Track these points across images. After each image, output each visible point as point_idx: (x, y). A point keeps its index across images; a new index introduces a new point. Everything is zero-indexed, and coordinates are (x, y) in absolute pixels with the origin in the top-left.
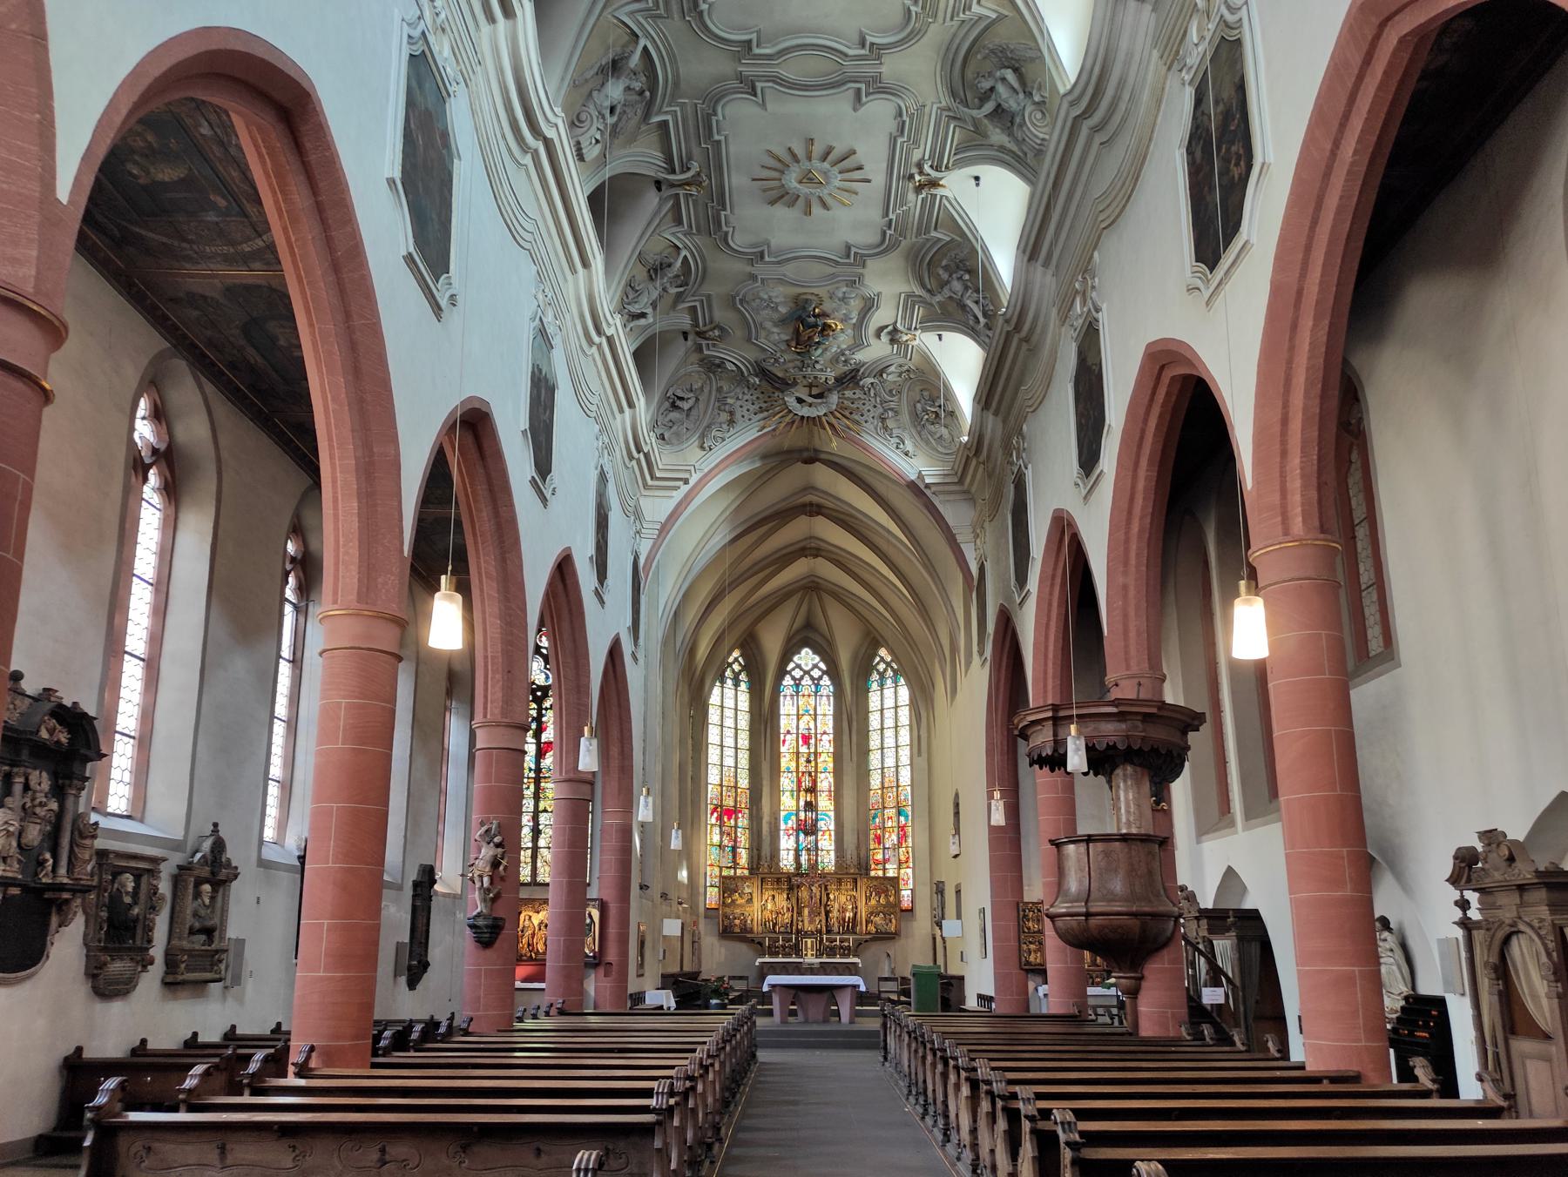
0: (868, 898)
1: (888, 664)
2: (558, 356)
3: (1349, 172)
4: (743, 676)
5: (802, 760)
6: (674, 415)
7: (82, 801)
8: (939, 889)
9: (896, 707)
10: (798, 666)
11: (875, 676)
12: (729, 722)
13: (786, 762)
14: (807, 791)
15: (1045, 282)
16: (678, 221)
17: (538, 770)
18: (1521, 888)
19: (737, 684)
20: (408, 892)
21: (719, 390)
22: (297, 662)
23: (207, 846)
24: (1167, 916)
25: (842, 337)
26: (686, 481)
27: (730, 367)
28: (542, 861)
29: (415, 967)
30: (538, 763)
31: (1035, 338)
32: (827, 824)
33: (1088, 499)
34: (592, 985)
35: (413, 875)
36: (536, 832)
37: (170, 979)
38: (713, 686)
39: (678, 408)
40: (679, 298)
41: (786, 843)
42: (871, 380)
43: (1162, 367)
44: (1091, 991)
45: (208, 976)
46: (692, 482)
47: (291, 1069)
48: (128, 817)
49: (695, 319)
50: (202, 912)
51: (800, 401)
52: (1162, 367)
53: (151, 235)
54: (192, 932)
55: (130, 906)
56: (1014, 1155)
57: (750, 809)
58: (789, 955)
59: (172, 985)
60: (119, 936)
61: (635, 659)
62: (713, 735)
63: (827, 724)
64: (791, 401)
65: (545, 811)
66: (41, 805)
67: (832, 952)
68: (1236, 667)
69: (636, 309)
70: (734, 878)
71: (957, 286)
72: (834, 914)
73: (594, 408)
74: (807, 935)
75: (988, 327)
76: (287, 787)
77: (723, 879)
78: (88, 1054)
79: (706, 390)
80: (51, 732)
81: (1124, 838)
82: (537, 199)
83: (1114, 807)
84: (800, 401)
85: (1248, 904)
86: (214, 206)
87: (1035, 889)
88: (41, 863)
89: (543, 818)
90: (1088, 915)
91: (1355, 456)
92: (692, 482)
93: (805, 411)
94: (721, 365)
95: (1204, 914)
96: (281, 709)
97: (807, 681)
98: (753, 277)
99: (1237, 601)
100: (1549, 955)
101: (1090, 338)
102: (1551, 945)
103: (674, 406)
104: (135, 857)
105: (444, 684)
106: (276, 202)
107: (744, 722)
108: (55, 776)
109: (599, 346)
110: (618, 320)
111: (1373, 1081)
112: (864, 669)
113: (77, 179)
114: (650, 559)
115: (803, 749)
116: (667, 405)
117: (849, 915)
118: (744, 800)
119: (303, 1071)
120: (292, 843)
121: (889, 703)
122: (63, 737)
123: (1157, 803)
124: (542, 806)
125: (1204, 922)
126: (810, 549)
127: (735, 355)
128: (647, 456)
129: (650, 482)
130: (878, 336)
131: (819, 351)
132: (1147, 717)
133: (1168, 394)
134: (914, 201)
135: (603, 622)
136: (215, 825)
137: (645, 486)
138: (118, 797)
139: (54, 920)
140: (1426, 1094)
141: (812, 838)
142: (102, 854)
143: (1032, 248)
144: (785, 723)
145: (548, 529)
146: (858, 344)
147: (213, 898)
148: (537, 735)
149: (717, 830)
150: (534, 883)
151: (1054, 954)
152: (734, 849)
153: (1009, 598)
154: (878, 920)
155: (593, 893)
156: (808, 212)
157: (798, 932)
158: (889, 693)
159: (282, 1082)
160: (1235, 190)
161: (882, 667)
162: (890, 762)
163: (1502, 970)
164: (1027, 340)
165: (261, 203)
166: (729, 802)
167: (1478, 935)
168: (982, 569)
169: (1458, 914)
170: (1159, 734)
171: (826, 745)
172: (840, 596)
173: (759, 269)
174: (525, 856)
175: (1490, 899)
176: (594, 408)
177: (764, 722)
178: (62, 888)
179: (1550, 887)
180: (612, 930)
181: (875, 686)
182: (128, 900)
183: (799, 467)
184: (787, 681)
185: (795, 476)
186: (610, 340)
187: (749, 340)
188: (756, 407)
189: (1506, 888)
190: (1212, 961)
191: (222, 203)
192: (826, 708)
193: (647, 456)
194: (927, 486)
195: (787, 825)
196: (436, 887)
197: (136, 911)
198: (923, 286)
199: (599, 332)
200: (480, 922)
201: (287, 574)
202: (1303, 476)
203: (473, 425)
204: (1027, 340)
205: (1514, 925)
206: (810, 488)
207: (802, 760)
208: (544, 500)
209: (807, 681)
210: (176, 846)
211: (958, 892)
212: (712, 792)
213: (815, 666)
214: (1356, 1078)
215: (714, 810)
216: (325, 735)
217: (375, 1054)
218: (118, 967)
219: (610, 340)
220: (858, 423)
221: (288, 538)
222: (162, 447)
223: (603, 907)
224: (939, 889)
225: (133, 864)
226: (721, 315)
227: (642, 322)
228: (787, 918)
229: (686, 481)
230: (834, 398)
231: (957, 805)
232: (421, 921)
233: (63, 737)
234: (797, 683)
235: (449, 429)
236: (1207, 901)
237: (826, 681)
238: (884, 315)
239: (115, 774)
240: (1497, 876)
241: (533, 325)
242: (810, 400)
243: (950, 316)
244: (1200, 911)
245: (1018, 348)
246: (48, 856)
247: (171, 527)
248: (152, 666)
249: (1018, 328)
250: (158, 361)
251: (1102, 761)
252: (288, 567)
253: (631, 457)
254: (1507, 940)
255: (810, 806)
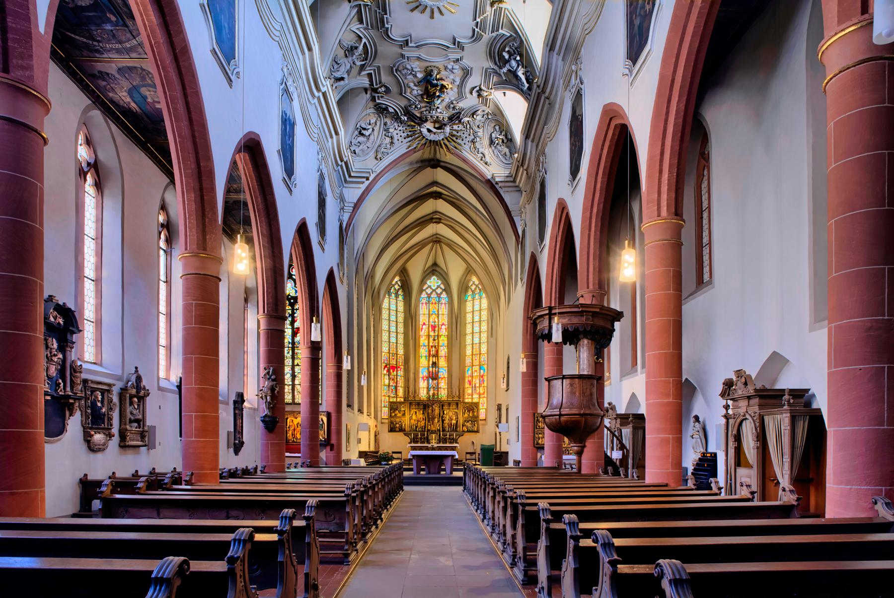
0: (464, 413)
1: (477, 286)
2: (296, 104)
3: (699, 13)
4: (400, 292)
5: (431, 339)
6: (361, 139)
7: (73, 354)
8: (499, 408)
9: (480, 310)
10: (430, 287)
11: (470, 293)
12: (393, 318)
13: (423, 341)
14: (434, 356)
15: (557, 61)
16: (361, 21)
17: (293, 343)
18: (749, 398)
19: (397, 296)
20: (232, 406)
21: (385, 124)
22: (168, 282)
23: (133, 378)
24: (597, 416)
25: (451, 93)
26: (367, 179)
27: (391, 110)
28: (296, 389)
29: (238, 447)
30: (293, 339)
31: (552, 97)
32: (443, 373)
33: (572, 193)
34: (323, 455)
35: (233, 397)
36: (294, 376)
37: (122, 444)
38: (384, 297)
39: (363, 135)
40: (362, 67)
41: (423, 384)
42: (467, 119)
43: (611, 119)
44: (565, 457)
45: (140, 443)
46: (371, 179)
47: (183, 483)
48: (95, 363)
49: (371, 81)
50: (135, 412)
51: (429, 131)
52: (611, 119)
53: (77, 37)
54: (131, 421)
55: (101, 408)
56: (514, 527)
57: (404, 366)
58: (423, 442)
59: (124, 445)
60: (96, 420)
61: (342, 282)
62: (385, 325)
63: (444, 319)
64: (424, 131)
65: (298, 365)
66: (55, 355)
67: (445, 441)
68: (623, 286)
69: (338, 75)
70: (395, 403)
71: (514, 63)
72: (447, 421)
73: (277, 33)
74: (433, 432)
75: (529, 89)
76: (169, 348)
77: (391, 403)
78: (90, 478)
79: (378, 124)
80: (55, 318)
81: (580, 377)
82: (282, 10)
83: (578, 360)
84: (429, 131)
85: (640, 412)
86: (109, 21)
87: (542, 409)
88: (58, 385)
89: (297, 369)
90: (560, 415)
91: (706, 173)
92: (371, 179)
93: (432, 137)
94: (386, 109)
95: (620, 416)
96: (163, 308)
97: (434, 295)
98: (403, 56)
99: (623, 252)
100: (756, 429)
101: (578, 98)
102: (757, 424)
103: (361, 134)
104: (100, 383)
105: (243, 296)
106: (143, 20)
107: (401, 319)
108: (58, 341)
109: (319, 98)
110: (328, 83)
111: (672, 485)
112: (464, 288)
113: (47, 19)
114: (349, 225)
115: (432, 333)
116: (357, 133)
117: (454, 422)
118: (401, 361)
119: (188, 483)
120: (174, 378)
121: (477, 308)
122: (61, 321)
123: (597, 359)
124: (296, 362)
125: (619, 420)
126: (434, 218)
127: (393, 103)
128: (346, 163)
129: (348, 179)
130: (471, 93)
131: (439, 101)
132: (594, 314)
133: (613, 134)
134: (489, 11)
135: (325, 259)
136: (136, 368)
137: (346, 181)
138: (89, 354)
139: (67, 413)
140: (692, 490)
141: (435, 382)
142: (85, 381)
143: (551, 45)
144: (422, 319)
145: (294, 206)
146: (461, 96)
147: (138, 405)
148: (293, 323)
149: (387, 377)
150: (294, 403)
151: (548, 438)
152: (396, 387)
153: (536, 249)
154: (468, 424)
155: (323, 408)
156: (432, 17)
157: (428, 430)
158: (477, 302)
159: (180, 487)
160: (647, 16)
161: (473, 287)
162: (476, 340)
163: (738, 438)
164: (548, 98)
165: (134, 19)
166: (393, 362)
167: (731, 421)
168: (524, 231)
169: (724, 411)
170: (599, 322)
171: (444, 332)
172: (451, 245)
173: (407, 52)
174: (287, 389)
175: (736, 403)
176: (316, 136)
177: (411, 317)
178: (69, 397)
179: (761, 397)
180: (333, 427)
181: (470, 298)
182: (99, 404)
183: (429, 170)
184: (424, 295)
185: (429, 174)
186: (324, 94)
187: (401, 94)
188: (405, 134)
189: (742, 398)
190: (620, 440)
191: (113, 19)
192: (444, 310)
193: (346, 163)
194: (497, 183)
195: (423, 373)
196: (245, 404)
197: (104, 410)
198: (496, 64)
199: (318, 89)
200: (267, 419)
201: (160, 233)
202: (668, 185)
203: (252, 147)
204: (548, 98)
205: (744, 415)
206: (435, 183)
207: (431, 339)
208: (290, 191)
209: (434, 295)
210: (119, 379)
211: (507, 409)
212: (384, 356)
213: (438, 287)
214: (666, 485)
215: (386, 366)
216: (186, 321)
217: (221, 478)
218: (98, 437)
219: (324, 94)
220: (460, 144)
221: (159, 213)
222: (92, 161)
223: (329, 415)
224: (499, 408)
225: (100, 387)
226: (386, 79)
227: (342, 83)
228: (423, 423)
229: (367, 179)
230: (448, 129)
231: (508, 363)
232: (239, 422)
233: (61, 321)
234: (429, 296)
235: (238, 150)
236: (621, 409)
237: (444, 295)
238: (475, 80)
239: (87, 341)
240: (740, 392)
241: (282, 87)
242: (434, 130)
243: (511, 82)
244: (617, 415)
245: (544, 102)
246: (60, 381)
247: (100, 207)
248: (98, 281)
249: (543, 92)
250: (87, 110)
251: (571, 336)
252: (160, 229)
253: (337, 165)
254: (741, 424)
255: (434, 364)
